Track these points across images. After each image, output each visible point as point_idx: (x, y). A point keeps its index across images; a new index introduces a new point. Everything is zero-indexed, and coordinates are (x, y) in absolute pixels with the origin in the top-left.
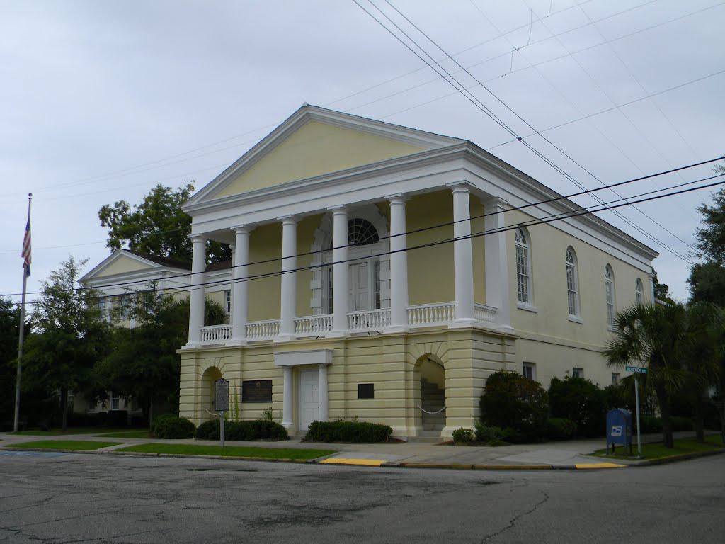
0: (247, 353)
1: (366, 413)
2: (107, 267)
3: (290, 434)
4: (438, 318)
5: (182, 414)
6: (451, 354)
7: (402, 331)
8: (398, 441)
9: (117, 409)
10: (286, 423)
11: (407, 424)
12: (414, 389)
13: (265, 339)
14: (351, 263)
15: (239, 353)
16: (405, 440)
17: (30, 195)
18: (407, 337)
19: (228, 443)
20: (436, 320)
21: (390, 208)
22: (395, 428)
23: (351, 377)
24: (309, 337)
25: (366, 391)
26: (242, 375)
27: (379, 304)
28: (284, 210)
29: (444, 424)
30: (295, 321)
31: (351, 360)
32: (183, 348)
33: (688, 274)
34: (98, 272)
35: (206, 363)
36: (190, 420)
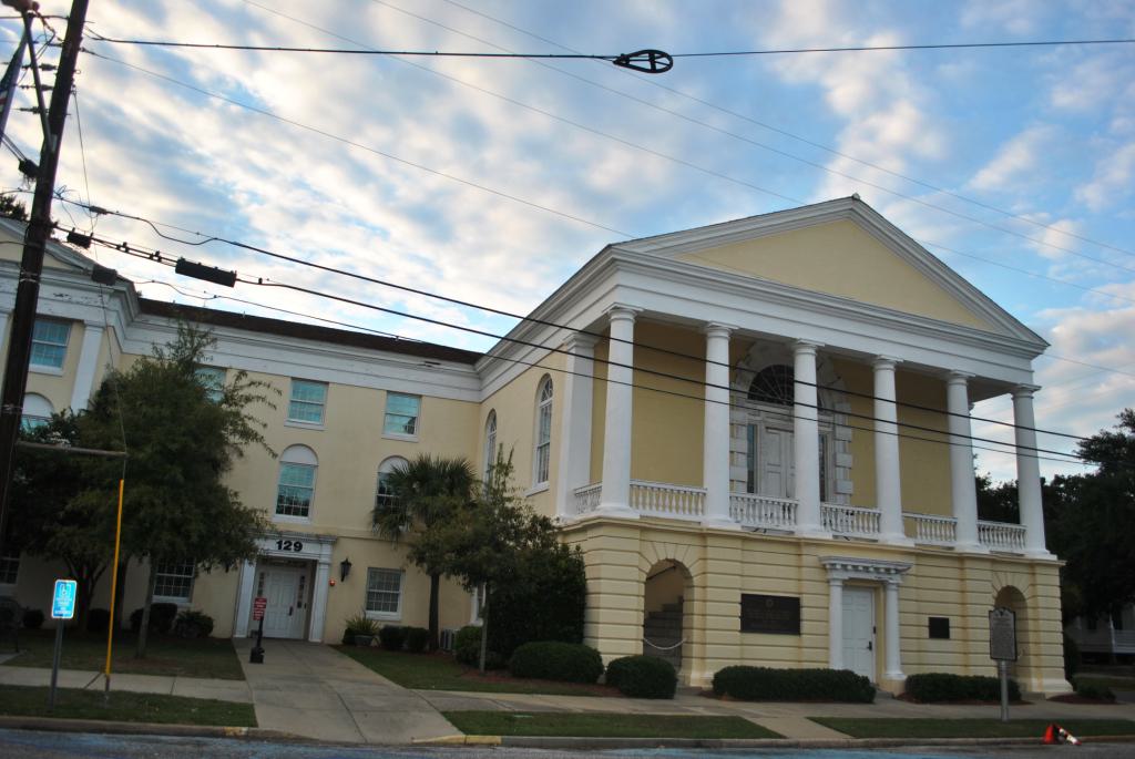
12: (1028, 631)
18: (644, 528)
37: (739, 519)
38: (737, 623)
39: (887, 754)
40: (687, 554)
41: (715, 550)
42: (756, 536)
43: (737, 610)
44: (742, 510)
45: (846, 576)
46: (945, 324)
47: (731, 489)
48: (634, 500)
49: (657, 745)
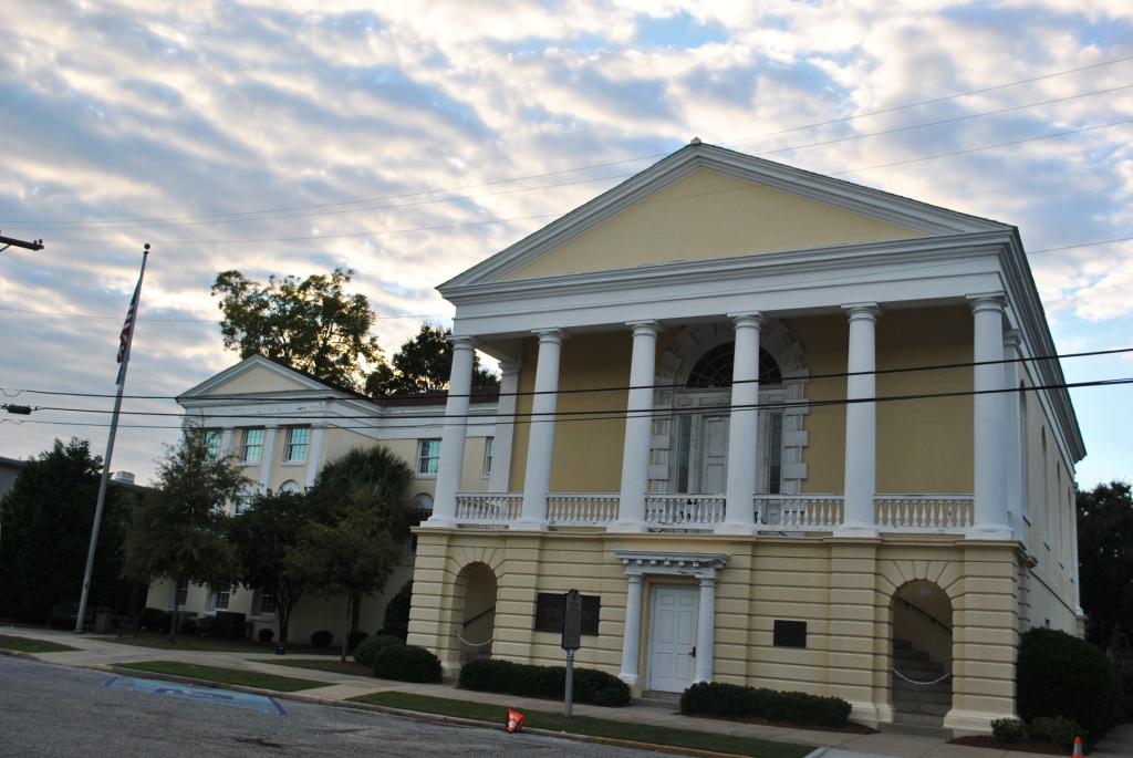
0: (551, 546)
1: (785, 673)
2: (229, 380)
3: (636, 694)
4: (598, 516)
5: (412, 640)
6: (969, 584)
7: (446, 526)
8: (861, 729)
9: (225, 610)
10: (627, 675)
11: (874, 700)
12: (453, 610)
13: (587, 525)
14: (656, 416)
15: (445, 541)
16: (875, 727)
17: (147, 246)
18: (882, 546)
19: (582, 710)
20: (602, 517)
21: (632, 340)
22: (856, 705)
23: (760, 607)
24: (475, 526)
25: (790, 634)
26: (538, 582)
27: (778, 485)
28: (641, 310)
29: (949, 705)
30: (548, 499)
31: (762, 577)
32: (423, 524)
33: (1107, 482)
34: (216, 387)
35: (467, 555)
36: (429, 650)
37: (663, 520)
38: (529, 621)
39: (640, 754)
40: (939, 573)
41: (513, 551)
42: (653, 536)
43: (531, 608)
44: (802, 513)
45: (640, 571)
46: (639, 270)
47: (649, 489)
48: (881, 515)
49: (488, 727)
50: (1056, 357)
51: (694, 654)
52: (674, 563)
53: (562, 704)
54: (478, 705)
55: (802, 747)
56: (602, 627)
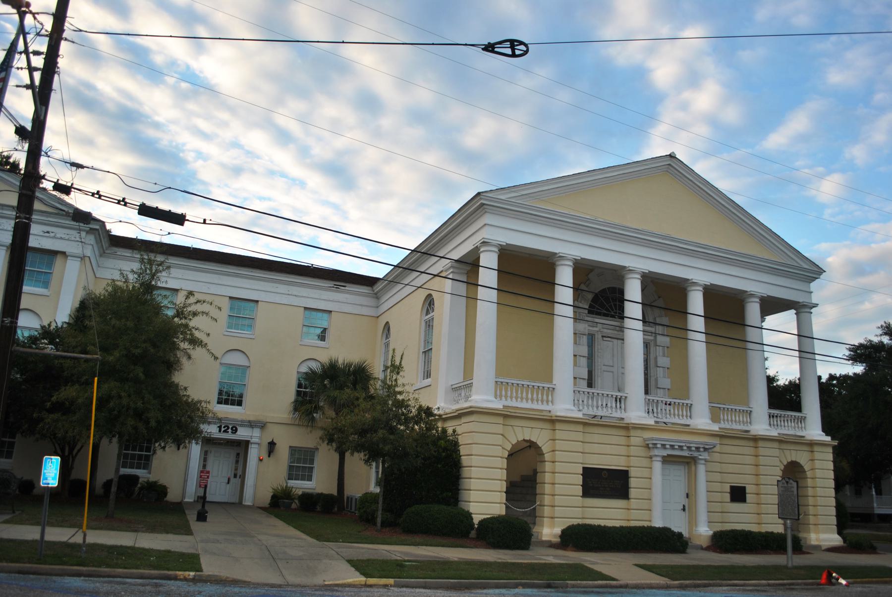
4: (678, 415)
18: (507, 416)
38: (579, 490)
40: (540, 436)
46: (637, 230)
47: (575, 384)
50: (705, 317)
51: (684, 510)
52: (672, 447)
53: (784, 557)
54: (764, 567)
55: (353, 566)
56: (633, 493)
